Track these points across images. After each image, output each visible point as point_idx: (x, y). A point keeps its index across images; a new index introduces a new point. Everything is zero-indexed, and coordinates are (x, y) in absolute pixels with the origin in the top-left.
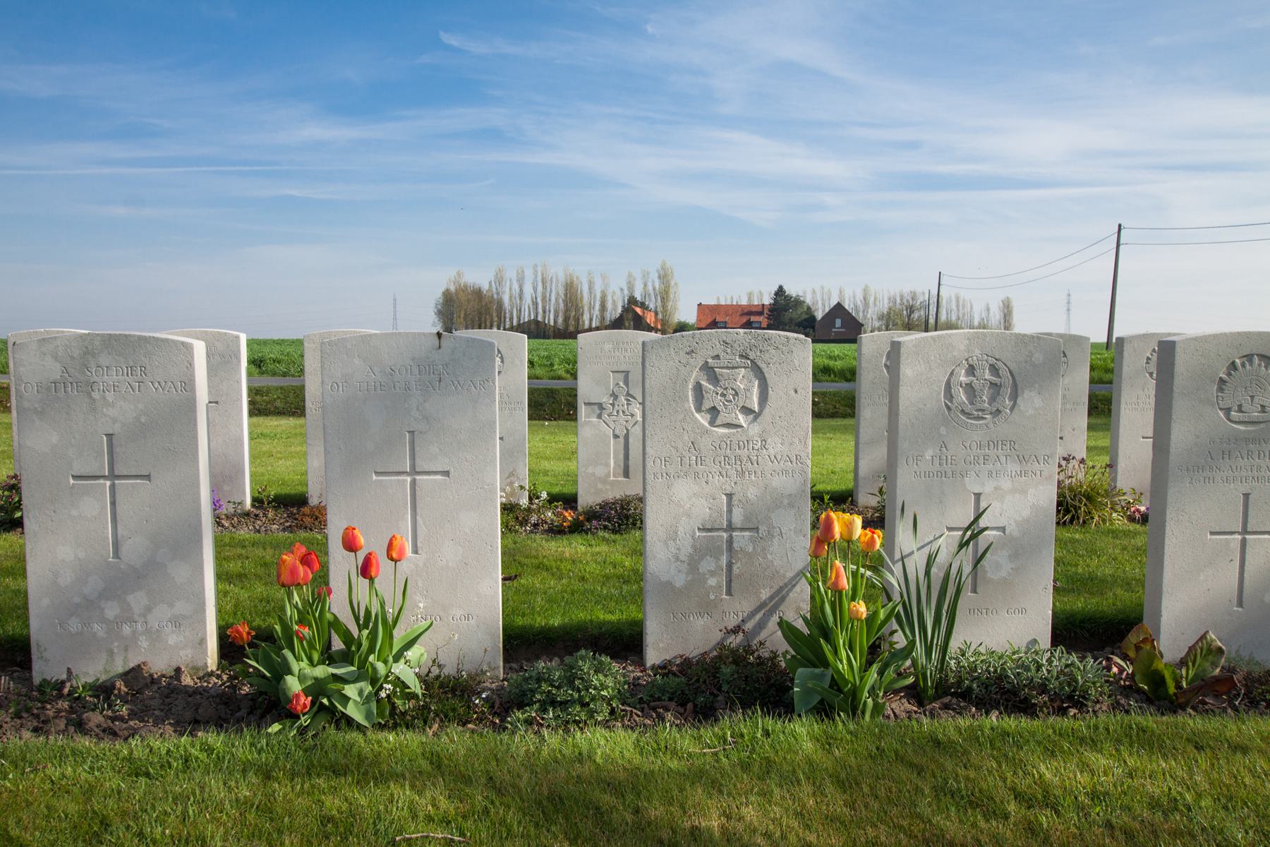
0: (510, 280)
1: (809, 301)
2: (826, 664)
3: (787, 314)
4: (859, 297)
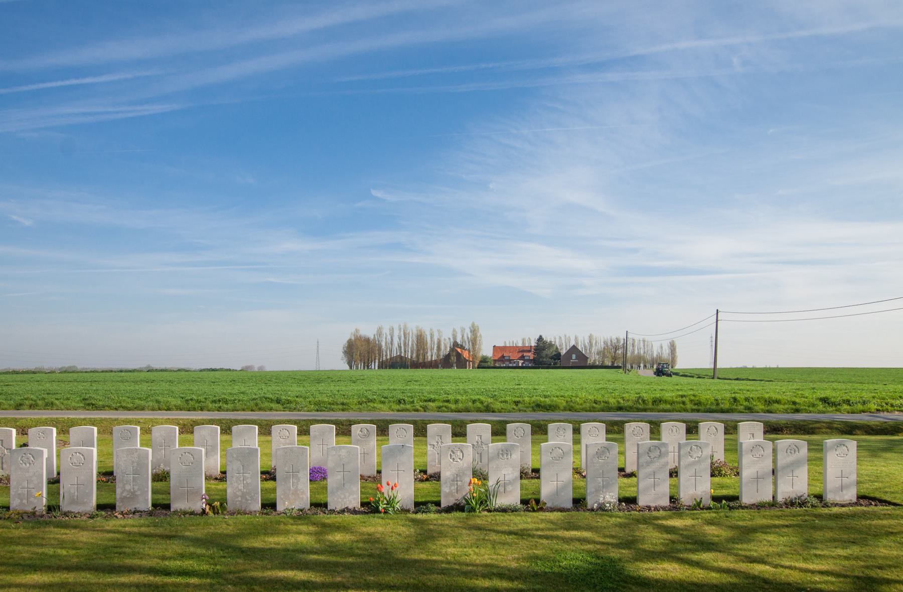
0: (386, 334)
1: (558, 344)
2: (470, 504)
3: (544, 352)
4: (587, 341)
